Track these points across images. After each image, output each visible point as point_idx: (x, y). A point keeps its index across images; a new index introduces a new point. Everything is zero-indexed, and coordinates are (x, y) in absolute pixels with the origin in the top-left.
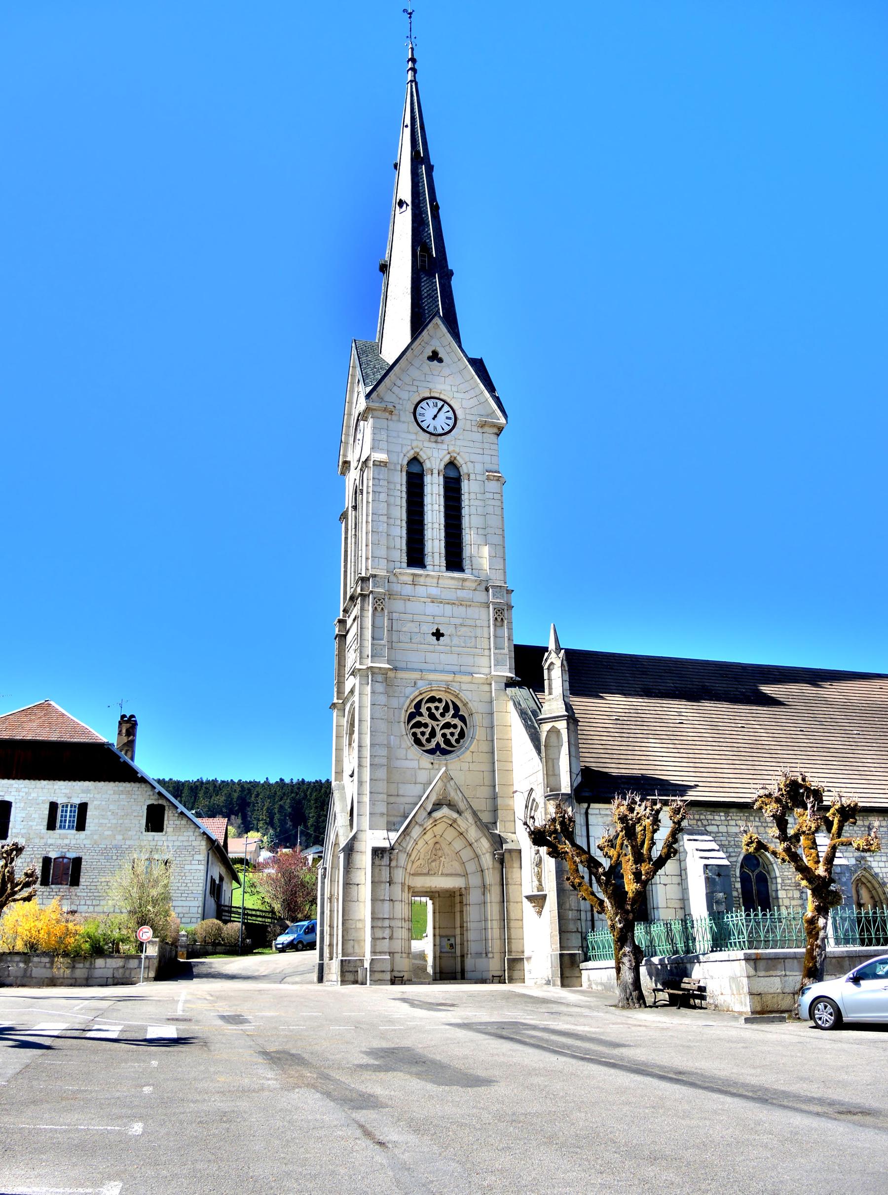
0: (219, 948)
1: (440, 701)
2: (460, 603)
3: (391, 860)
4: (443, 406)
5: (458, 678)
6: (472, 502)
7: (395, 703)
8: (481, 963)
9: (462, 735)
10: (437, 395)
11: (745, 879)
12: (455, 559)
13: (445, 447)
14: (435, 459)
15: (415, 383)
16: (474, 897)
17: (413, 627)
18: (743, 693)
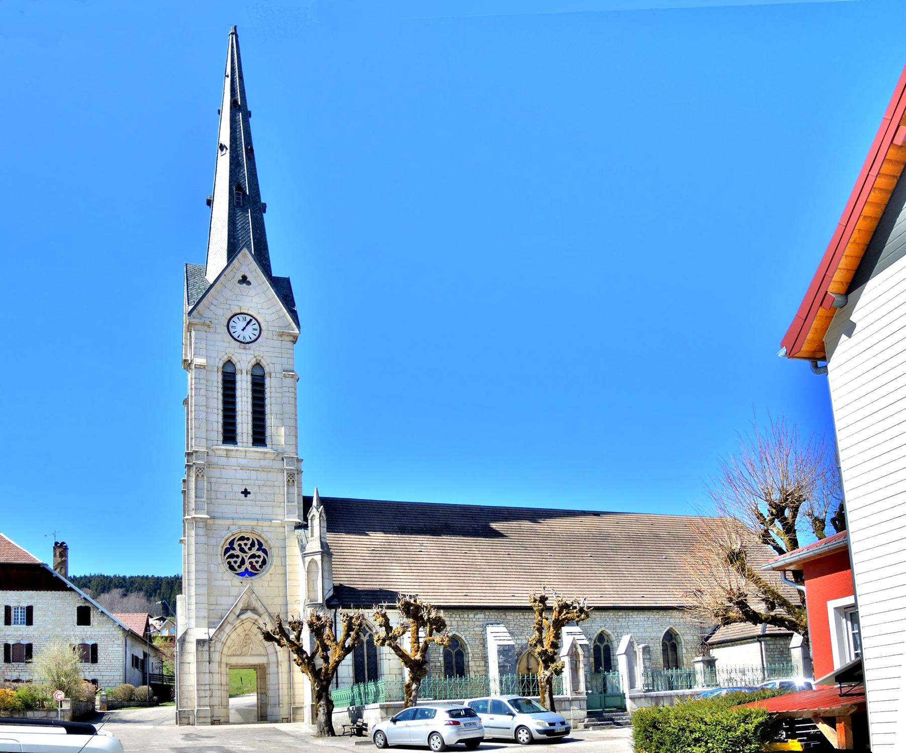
0: (132, 703)
1: (248, 539)
2: (263, 469)
3: (210, 647)
4: (251, 320)
5: (260, 523)
6: (273, 395)
7: (213, 541)
8: (276, 710)
9: (264, 562)
10: (246, 312)
11: (447, 655)
12: (259, 437)
13: (252, 352)
14: (244, 363)
15: (229, 302)
16: (272, 669)
17: (226, 488)
18: (474, 529)
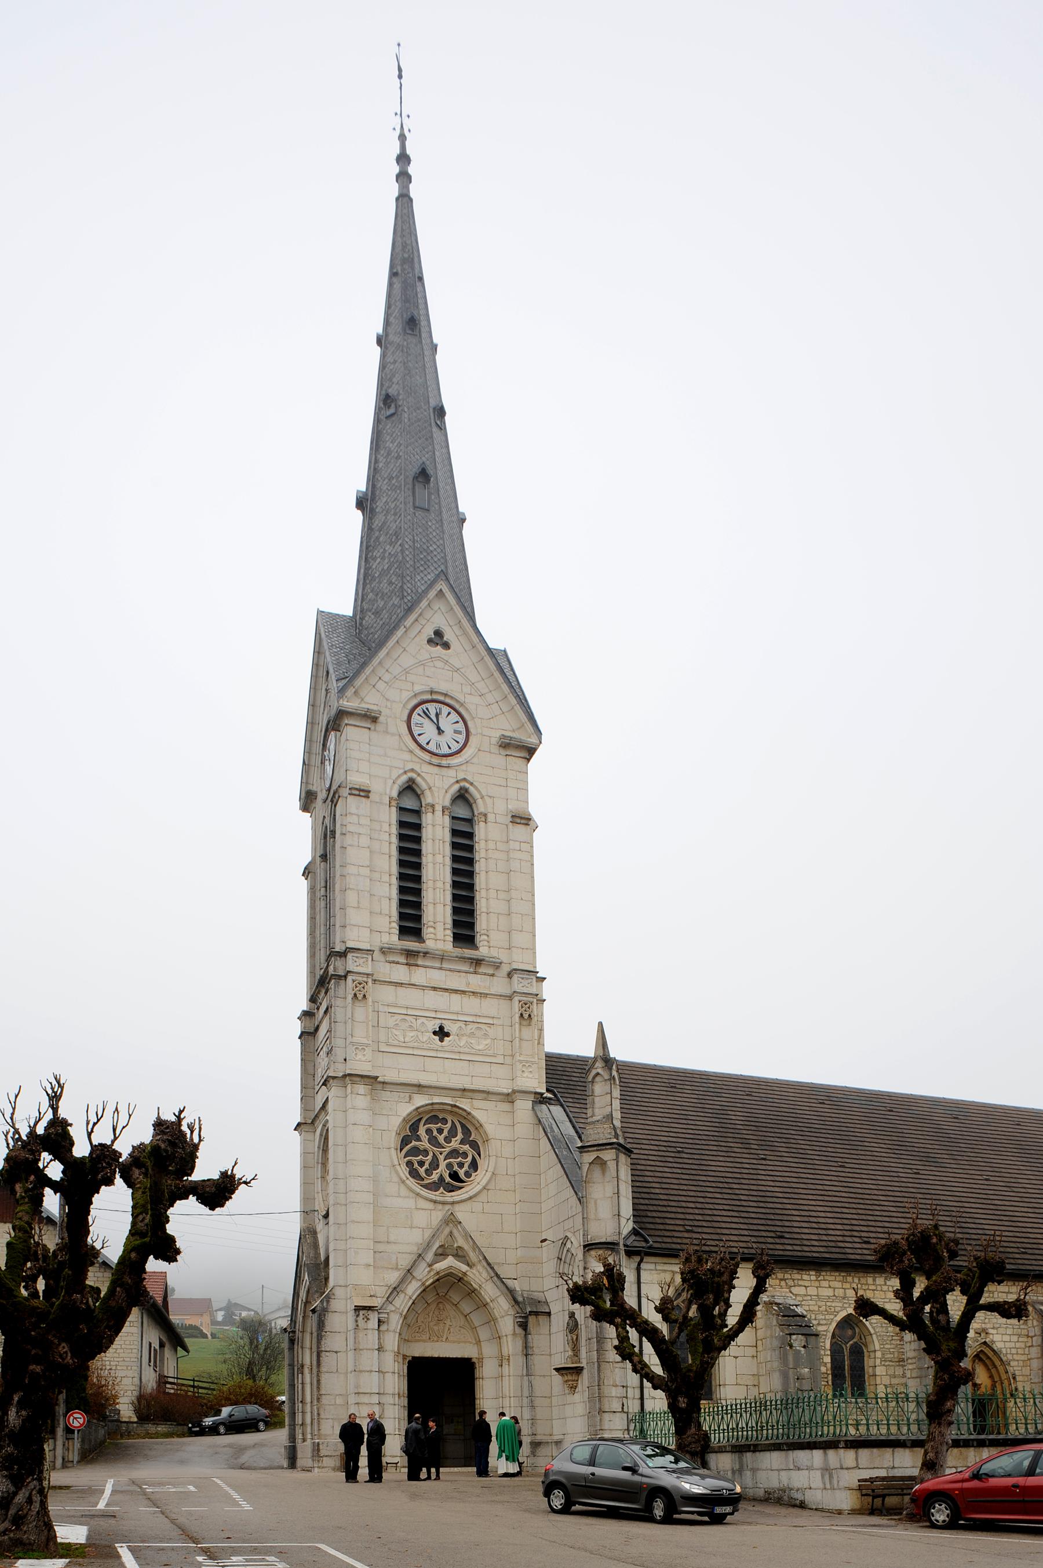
6: (490, 854)
12: (464, 930)
14: (437, 790)
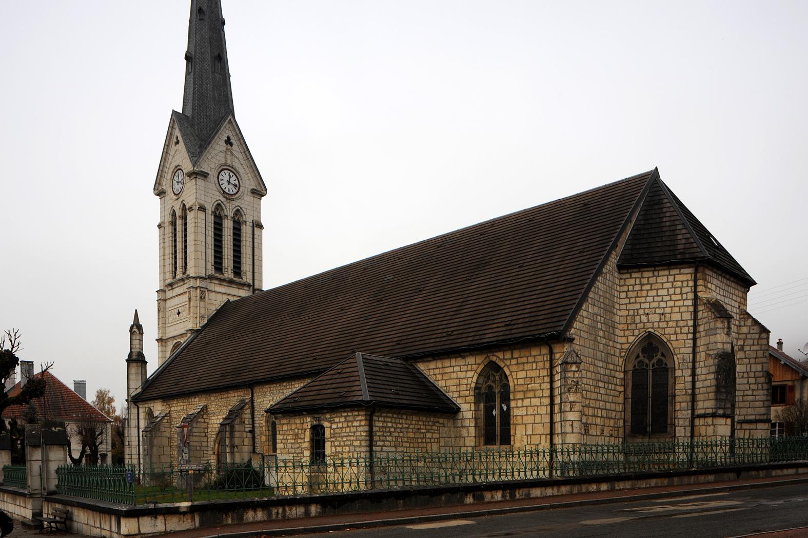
12: (237, 271)
14: (229, 211)
